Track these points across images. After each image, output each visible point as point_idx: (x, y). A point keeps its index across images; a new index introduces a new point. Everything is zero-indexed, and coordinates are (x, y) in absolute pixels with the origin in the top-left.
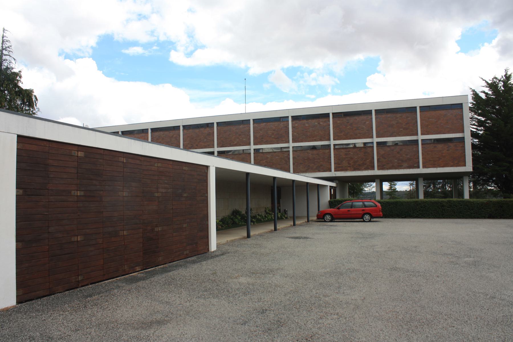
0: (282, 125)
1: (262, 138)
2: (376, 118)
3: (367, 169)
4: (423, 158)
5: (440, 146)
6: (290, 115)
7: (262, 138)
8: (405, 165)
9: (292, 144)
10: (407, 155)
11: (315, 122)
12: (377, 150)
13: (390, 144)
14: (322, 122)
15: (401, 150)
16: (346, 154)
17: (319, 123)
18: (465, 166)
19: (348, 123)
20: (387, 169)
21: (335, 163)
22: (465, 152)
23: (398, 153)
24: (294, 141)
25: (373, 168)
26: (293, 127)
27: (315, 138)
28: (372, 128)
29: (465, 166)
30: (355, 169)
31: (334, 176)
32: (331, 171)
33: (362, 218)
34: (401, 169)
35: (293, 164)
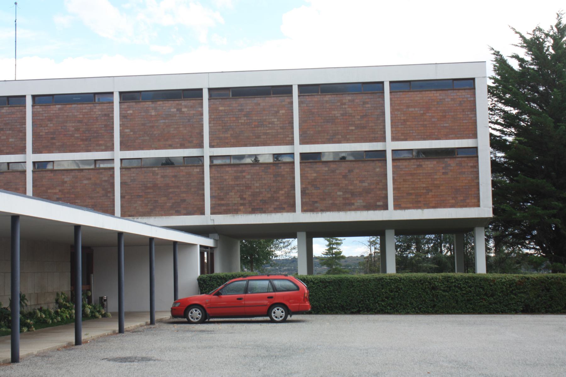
0: (97, 110)
2: (300, 103)
3: (279, 209)
5: (429, 165)
6: (117, 90)
7: (53, 138)
8: (359, 202)
9: (390, 145)
10: (362, 181)
11: (170, 106)
12: (301, 170)
14: (186, 107)
15: (350, 171)
16: (237, 178)
17: (179, 110)
18: (479, 206)
19: (241, 110)
21: (212, 197)
23: (345, 177)
24: (125, 146)
25: (292, 208)
27: (170, 143)
28: (291, 123)
29: (479, 206)
30: (254, 210)
31: (210, 223)
33: (268, 314)
34: (350, 210)
35: (122, 197)
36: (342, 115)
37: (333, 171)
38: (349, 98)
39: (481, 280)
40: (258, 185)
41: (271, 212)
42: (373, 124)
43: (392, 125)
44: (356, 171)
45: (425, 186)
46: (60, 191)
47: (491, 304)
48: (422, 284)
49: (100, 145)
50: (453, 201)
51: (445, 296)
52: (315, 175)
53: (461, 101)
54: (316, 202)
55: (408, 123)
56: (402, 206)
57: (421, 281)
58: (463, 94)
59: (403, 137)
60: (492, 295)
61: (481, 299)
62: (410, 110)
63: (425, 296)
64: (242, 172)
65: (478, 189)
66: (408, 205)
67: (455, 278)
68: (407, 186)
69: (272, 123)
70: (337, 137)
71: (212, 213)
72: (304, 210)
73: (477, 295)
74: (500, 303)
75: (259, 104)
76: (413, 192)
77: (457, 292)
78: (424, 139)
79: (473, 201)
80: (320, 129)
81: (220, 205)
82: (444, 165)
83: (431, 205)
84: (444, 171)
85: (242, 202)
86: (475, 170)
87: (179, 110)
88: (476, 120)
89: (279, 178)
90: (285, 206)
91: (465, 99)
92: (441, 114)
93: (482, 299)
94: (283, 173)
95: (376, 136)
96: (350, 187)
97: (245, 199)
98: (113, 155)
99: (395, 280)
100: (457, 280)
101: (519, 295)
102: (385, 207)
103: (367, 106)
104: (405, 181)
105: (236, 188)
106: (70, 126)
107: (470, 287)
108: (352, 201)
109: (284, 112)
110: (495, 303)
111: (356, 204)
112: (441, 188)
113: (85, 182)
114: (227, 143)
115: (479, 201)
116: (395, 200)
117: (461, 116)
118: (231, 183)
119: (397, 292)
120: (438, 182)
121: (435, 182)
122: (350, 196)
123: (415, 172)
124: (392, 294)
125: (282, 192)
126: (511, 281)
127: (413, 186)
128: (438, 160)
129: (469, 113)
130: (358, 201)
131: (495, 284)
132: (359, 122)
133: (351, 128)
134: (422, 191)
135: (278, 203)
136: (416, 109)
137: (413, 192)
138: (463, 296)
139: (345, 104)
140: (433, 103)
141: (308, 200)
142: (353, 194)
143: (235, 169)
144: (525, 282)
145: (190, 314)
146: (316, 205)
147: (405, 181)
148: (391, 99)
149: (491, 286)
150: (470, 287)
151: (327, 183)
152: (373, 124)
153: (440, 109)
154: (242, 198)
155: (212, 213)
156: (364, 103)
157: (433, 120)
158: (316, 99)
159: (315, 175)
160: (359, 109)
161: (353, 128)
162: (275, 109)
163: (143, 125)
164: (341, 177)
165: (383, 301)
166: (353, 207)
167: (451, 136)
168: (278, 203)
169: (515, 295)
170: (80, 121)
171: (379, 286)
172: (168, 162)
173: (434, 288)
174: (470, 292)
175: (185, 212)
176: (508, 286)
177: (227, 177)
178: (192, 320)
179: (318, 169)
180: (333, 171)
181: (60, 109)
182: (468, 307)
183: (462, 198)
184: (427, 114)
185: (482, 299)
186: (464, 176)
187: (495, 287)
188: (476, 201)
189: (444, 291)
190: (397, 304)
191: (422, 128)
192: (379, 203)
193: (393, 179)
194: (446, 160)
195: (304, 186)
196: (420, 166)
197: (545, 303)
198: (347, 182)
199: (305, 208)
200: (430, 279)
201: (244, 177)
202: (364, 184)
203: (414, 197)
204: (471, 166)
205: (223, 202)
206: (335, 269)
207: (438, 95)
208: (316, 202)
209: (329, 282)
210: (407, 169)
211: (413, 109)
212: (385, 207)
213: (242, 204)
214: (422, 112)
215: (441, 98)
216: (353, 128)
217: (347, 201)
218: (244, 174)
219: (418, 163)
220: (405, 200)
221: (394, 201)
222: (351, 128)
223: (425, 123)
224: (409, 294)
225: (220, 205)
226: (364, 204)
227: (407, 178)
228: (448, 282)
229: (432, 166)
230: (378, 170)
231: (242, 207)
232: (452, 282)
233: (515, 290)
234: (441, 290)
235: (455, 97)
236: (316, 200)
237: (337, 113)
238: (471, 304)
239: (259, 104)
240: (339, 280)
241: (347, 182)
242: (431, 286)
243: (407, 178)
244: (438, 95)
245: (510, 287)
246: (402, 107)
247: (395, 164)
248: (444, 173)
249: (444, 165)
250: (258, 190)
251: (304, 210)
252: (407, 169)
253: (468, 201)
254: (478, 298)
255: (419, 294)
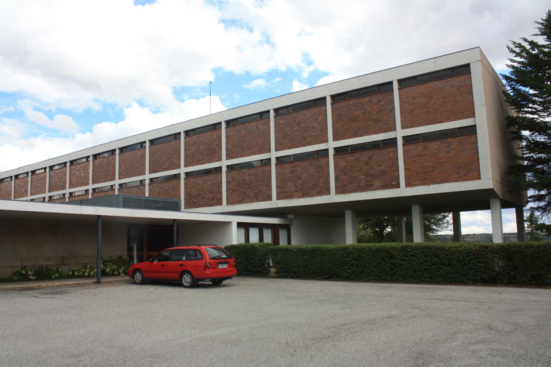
1: (194, 157)
2: (333, 109)
3: (320, 193)
4: (405, 170)
7: (194, 157)
8: (378, 183)
10: (379, 166)
12: (335, 161)
13: (107, 189)
15: (371, 158)
16: (292, 172)
18: (480, 178)
20: (351, 192)
21: (277, 187)
22: (478, 153)
23: (366, 163)
26: (227, 137)
27: (252, 151)
29: (479, 178)
30: (304, 195)
31: (275, 206)
32: (221, 204)
34: (371, 190)
35: (227, 191)
36: (363, 113)
37: (358, 160)
38: (367, 99)
39: (436, 250)
40: (305, 175)
41: (315, 196)
42: (386, 118)
43: (401, 116)
44: (375, 157)
45: (430, 164)
46: (197, 190)
47: (448, 273)
48: (380, 253)
49: (215, 158)
50: (457, 176)
51: (403, 265)
52: (344, 164)
53: (459, 86)
54: (346, 185)
55: (414, 112)
56: (412, 183)
57: (379, 250)
58: (461, 79)
59: (410, 125)
60: (449, 265)
61: (437, 268)
62: (416, 100)
63: (384, 265)
64: (295, 167)
65: (479, 162)
66: (417, 183)
67: (411, 248)
68: (416, 166)
69: (314, 127)
70: (360, 131)
71: (277, 199)
72: (337, 193)
73: (433, 265)
74: (458, 273)
75: (305, 115)
76: (421, 170)
77: (414, 261)
78: (429, 124)
79: (475, 174)
80: (347, 127)
81: (282, 193)
82: (447, 145)
83: (437, 181)
84: (447, 150)
85: (296, 189)
86: (475, 146)
87: (258, 128)
88: (473, 100)
89: (320, 169)
90: (324, 190)
91: (463, 84)
92: (442, 100)
93: (440, 268)
94: (322, 165)
95: (390, 126)
96: (370, 171)
97: (297, 187)
98: (396, 134)
99: (357, 249)
100: (413, 249)
101: (478, 265)
102: (398, 186)
103: (381, 103)
104: (414, 162)
105: (292, 179)
106: (202, 148)
107: (426, 256)
108: (373, 183)
109: (322, 118)
110: (452, 273)
111: (375, 185)
112: (445, 165)
113: (209, 183)
114: (286, 147)
115: (480, 175)
116: (227, 198)
117: (460, 99)
118: (289, 176)
119: (360, 260)
120: (443, 160)
121: (440, 161)
122: (371, 178)
123: (422, 153)
124: (355, 262)
125: (321, 180)
126: (468, 250)
127: (421, 166)
128: (441, 141)
129: (467, 95)
130: (377, 182)
131: (451, 253)
132: (376, 117)
133: (369, 123)
134: (428, 170)
135: (319, 189)
136: (421, 99)
137: (421, 170)
138: (420, 265)
139: (365, 104)
140: (435, 92)
141: (340, 184)
142: (373, 177)
143: (291, 165)
144: (484, 251)
145: (184, 280)
146: (346, 188)
147: (414, 162)
148: (400, 95)
149: (447, 255)
150: (426, 256)
151: (353, 169)
152: (386, 118)
153: (441, 96)
154: (295, 186)
155: (277, 199)
156: (379, 101)
157: (436, 106)
158: (344, 104)
159: (344, 164)
160: (375, 106)
161: (372, 123)
162: (316, 117)
163: (238, 141)
164: (364, 163)
165: (349, 268)
166: (373, 187)
167: (451, 118)
168: (319, 189)
169: (475, 265)
170: (206, 144)
171: (345, 255)
172: (249, 165)
173: (392, 257)
174: (427, 261)
175: (261, 199)
176: (465, 255)
177: (286, 172)
178: (185, 284)
179: (346, 159)
180: (358, 160)
181: (197, 138)
182: (425, 276)
183: (465, 173)
184: (431, 102)
185: (440, 268)
186: (465, 152)
187: (452, 256)
188: (477, 174)
189: (402, 260)
190: (361, 272)
191: (427, 115)
192: (393, 183)
193: (404, 161)
194: (448, 140)
195: (337, 174)
196: (426, 148)
197: (508, 274)
198: (368, 167)
199: (338, 191)
200: (388, 249)
201: (297, 170)
202: (381, 168)
203: (422, 175)
204: (472, 143)
205: (284, 190)
206: (535, 237)
207: (439, 84)
208: (346, 185)
209: (306, 251)
210: (415, 152)
211: (418, 100)
212: (398, 186)
213: (296, 191)
214: (426, 101)
215: (442, 86)
216: (372, 123)
217: (369, 183)
218: (297, 168)
219: (424, 145)
220: (414, 178)
221: (405, 180)
222: (369, 123)
223: (429, 110)
224: (370, 262)
225: (282, 193)
226: (382, 184)
227: (416, 159)
228: (405, 251)
229: (437, 146)
230: (392, 155)
231: (295, 193)
232: (409, 252)
233: (472, 259)
234: (399, 259)
235: (454, 83)
236: (345, 184)
237: (359, 113)
238: (429, 273)
239: (305, 115)
240: (313, 249)
241: (368, 167)
242: (389, 254)
243: (416, 159)
244: (439, 84)
245: (467, 256)
246: (409, 100)
247: (405, 148)
248: (448, 152)
249: (447, 145)
250: (305, 180)
251: (337, 193)
252: (415, 152)
253: (470, 175)
254: (435, 267)
255: (379, 263)
